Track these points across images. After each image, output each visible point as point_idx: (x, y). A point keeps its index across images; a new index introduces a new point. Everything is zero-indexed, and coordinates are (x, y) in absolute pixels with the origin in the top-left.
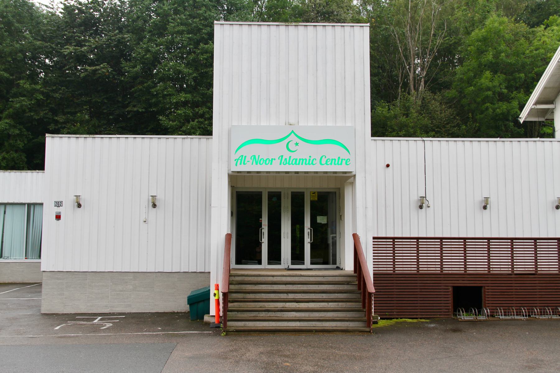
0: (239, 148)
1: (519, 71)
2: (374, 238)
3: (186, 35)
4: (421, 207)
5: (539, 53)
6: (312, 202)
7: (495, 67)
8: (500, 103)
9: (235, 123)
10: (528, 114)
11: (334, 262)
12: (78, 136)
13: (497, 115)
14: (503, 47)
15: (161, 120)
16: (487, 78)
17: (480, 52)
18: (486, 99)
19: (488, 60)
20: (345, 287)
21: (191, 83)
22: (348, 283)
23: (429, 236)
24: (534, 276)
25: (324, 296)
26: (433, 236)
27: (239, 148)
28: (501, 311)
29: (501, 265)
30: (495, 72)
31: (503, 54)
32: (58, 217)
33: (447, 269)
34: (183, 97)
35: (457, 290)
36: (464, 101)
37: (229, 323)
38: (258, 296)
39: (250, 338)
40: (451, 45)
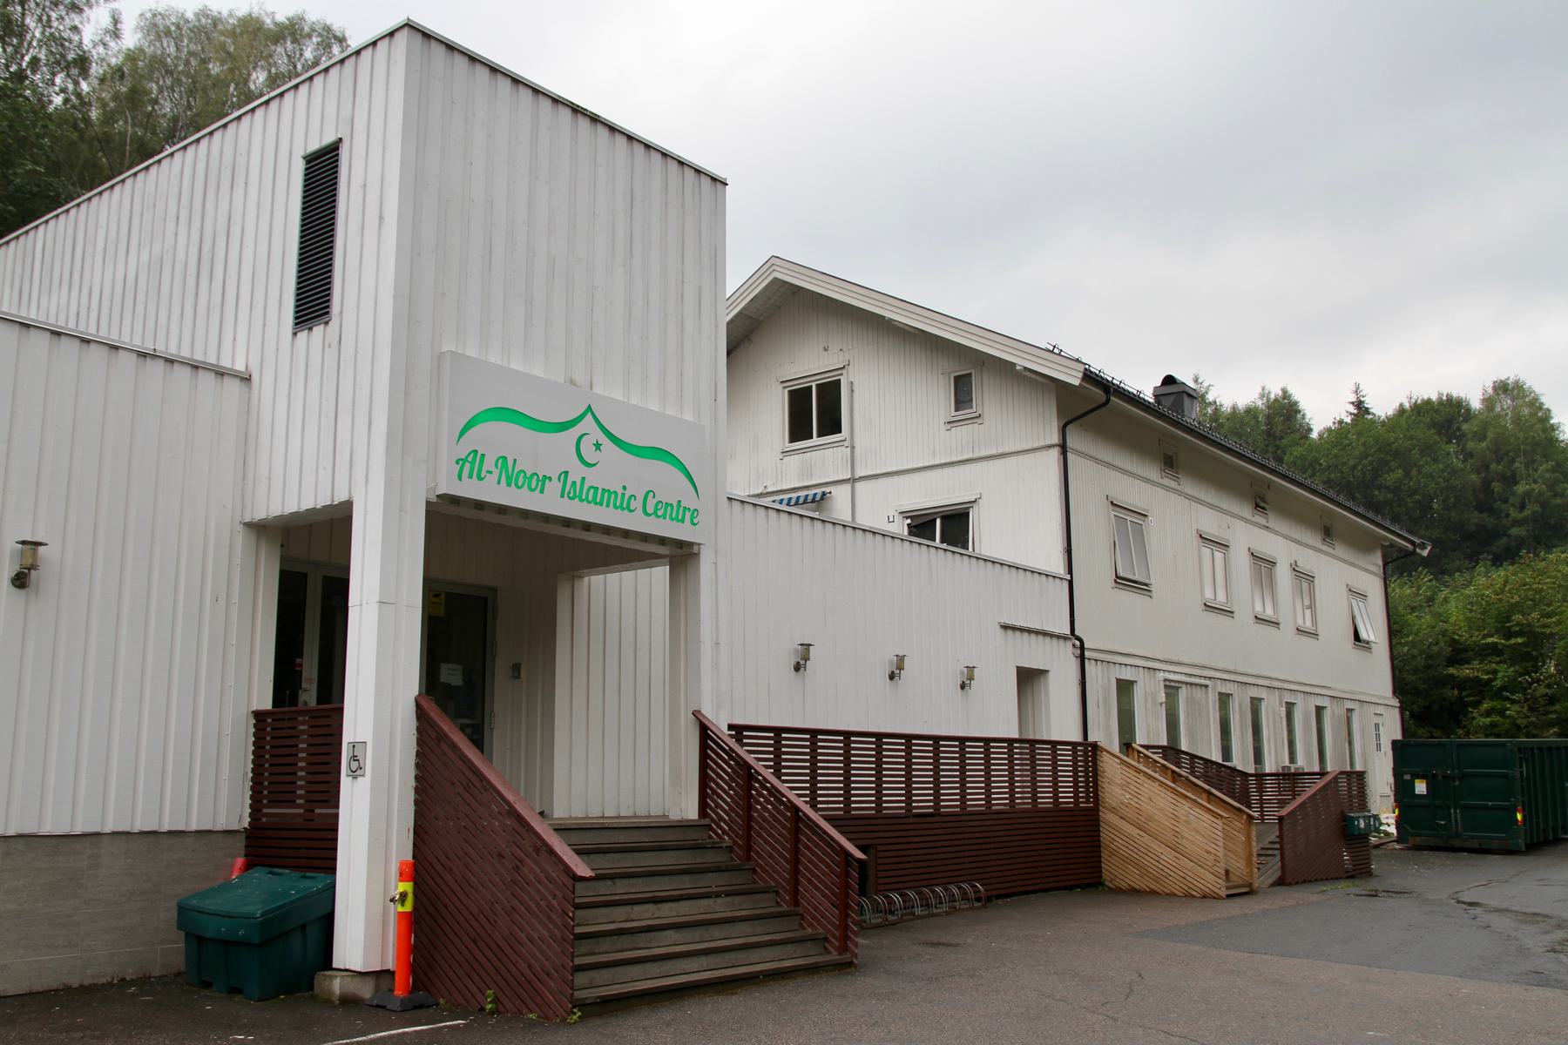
9: (447, 347)
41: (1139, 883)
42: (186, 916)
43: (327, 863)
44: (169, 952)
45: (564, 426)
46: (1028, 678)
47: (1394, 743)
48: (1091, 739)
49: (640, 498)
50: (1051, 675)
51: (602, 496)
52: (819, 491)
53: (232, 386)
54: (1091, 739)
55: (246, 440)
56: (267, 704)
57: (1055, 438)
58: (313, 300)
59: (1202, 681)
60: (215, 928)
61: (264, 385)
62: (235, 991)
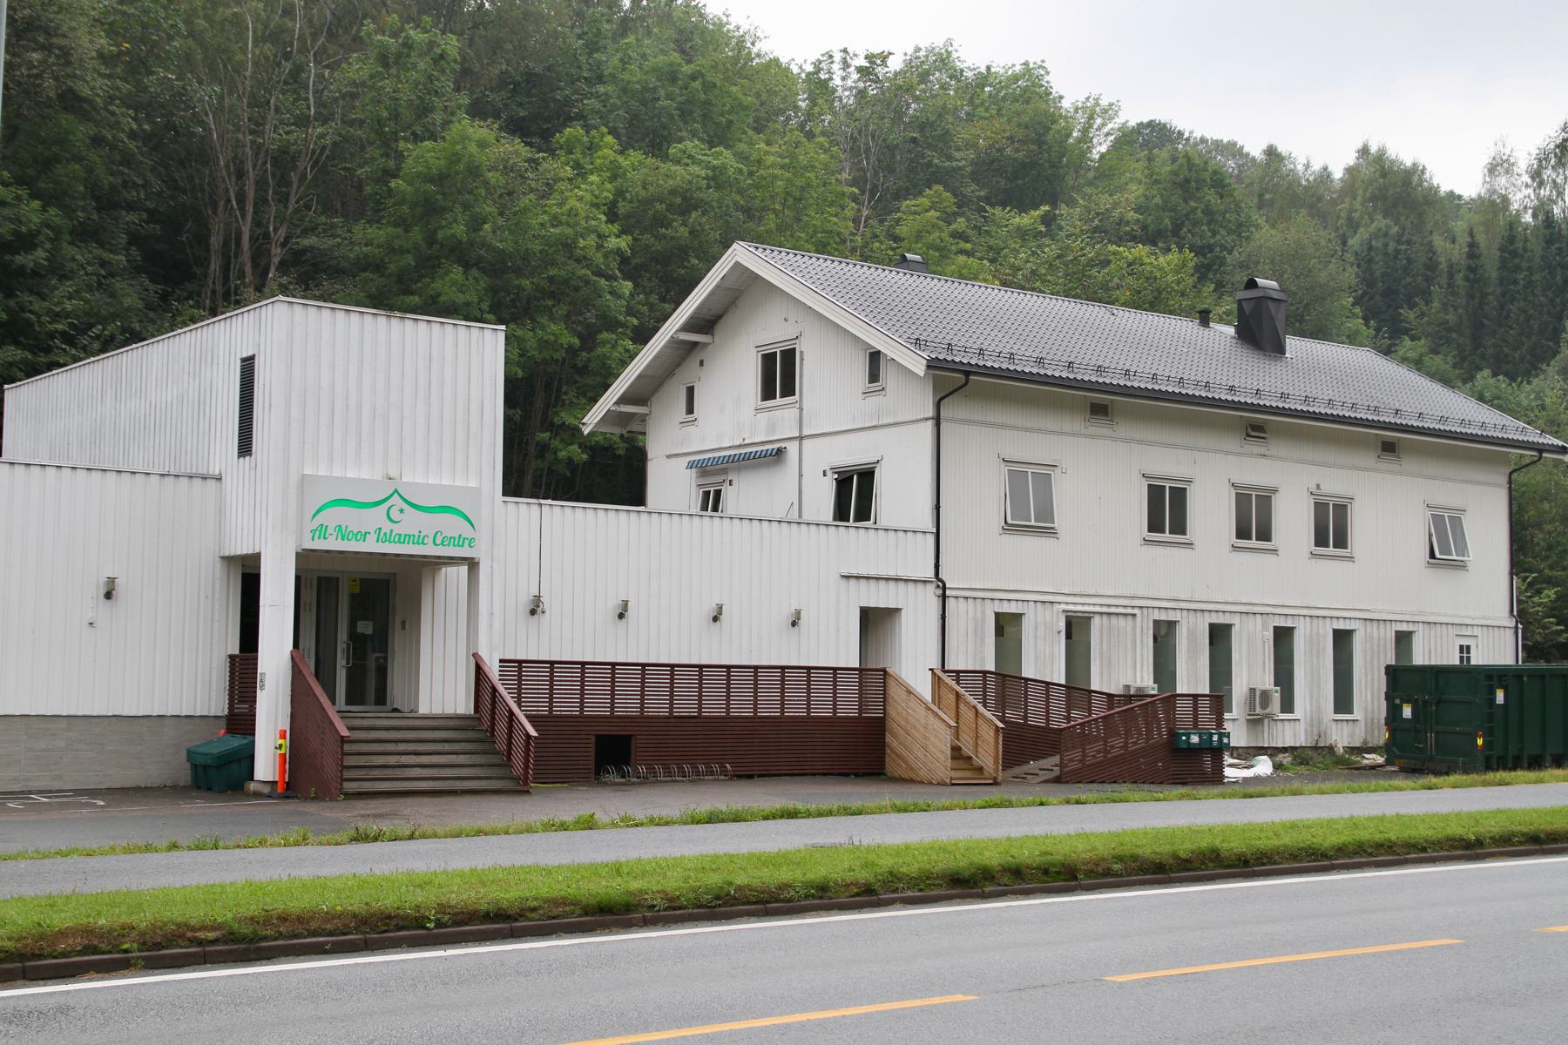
0: (318, 511)
1: (519, 272)
4: (533, 612)
6: (353, 596)
9: (308, 471)
11: (381, 699)
14: (488, 208)
16: (454, 283)
19: (453, 236)
20: (471, 735)
24: (697, 721)
25: (447, 747)
27: (318, 511)
28: (659, 768)
29: (657, 707)
35: (600, 739)
42: (191, 754)
43: (251, 731)
44: (184, 775)
46: (874, 622)
47: (1388, 668)
51: (408, 538)
52: (776, 446)
53: (211, 484)
55: (221, 511)
56: (236, 651)
57: (930, 412)
58: (245, 447)
59: (1129, 611)
60: (200, 760)
61: (227, 480)
62: (210, 789)
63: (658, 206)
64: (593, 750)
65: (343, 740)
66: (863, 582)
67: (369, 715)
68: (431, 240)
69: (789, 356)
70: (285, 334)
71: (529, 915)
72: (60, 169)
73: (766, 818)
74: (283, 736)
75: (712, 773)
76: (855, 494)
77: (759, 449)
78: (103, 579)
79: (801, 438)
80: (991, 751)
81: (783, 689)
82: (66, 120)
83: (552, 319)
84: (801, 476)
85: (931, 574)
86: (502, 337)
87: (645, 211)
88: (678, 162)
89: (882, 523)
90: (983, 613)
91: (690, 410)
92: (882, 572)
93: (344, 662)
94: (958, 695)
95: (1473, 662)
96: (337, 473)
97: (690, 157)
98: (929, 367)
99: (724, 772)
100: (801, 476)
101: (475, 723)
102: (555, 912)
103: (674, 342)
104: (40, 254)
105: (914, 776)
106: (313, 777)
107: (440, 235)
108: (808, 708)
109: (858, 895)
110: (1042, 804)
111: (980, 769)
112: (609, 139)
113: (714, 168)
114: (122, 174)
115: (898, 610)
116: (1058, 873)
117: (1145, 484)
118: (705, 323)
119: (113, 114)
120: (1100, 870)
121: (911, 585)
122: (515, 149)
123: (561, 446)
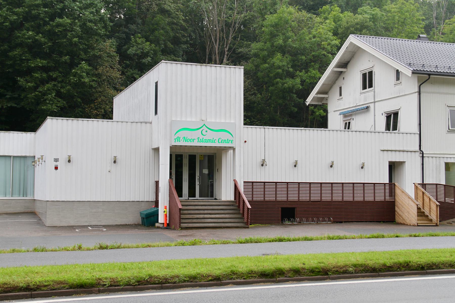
0: (177, 132)
1: (303, 54)
2: (244, 182)
3: (42, 9)
5: (315, 41)
7: (283, 50)
8: (287, 80)
9: (173, 119)
10: (312, 100)
11: (212, 196)
12: (68, 118)
13: (284, 89)
14: (290, 34)
15: (19, 81)
16: (278, 59)
17: (273, 36)
18: (278, 75)
19: (279, 44)
20: (232, 207)
21: (46, 51)
22: (233, 205)
23: (257, 181)
25: (222, 212)
26: (272, 181)
27: (177, 132)
28: (304, 219)
29: (304, 197)
30: (284, 53)
31: (290, 40)
32: (56, 168)
33: (279, 199)
34: (40, 62)
36: (260, 74)
37: (182, 224)
38: (189, 212)
39: (197, 230)
40: (246, 20)
41: (402, 222)
44: (138, 220)
45: (198, 129)
46: (393, 167)
48: (424, 183)
49: (217, 140)
50: (406, 163)
52: (366, 106)
53: (148, 125)
54: (424, 183)
57: (417, 90)
58: (156, 113)
63: (351, 29)
64: (280, 214)
65: (180, 209)
66: (389, 152)
67: (206, 201)
68: (272, 46)
69: (371, 73)
70: (168, 74)
71: (43, 288)
72: (156, 32)
73: (270, 241)
74: (166, 208)
75: (325, 221)
76: (392, 121)
77: (361, 107)
78: (113, 157)
79: (375, 102)
80: (435, 214)
81: (353, 191)
82: (159, 17)
83: (314, 69)
84: (375, 115)
85: (418, 149)
86: (242, 71)
87: (347, 31)
88: (361, 14)
89: (402, 130)
90: (440, 162)
91: (341, 95)
92: (397, 149)
93: (198, 183)
94: (423, 193)
95: (388, 182)
96: (184, 119)
97: (366, 12)
98: (413, 73)
99: (329, 220)
100: (375, 115)
101: (235, 203)
102: (56, 287)
103: (333, 72)
104: (149, 59)
105: (405, 223)
106: (179, 221)
107: (275, 44)
108: (354, 198)
109: (211, 280)
110: (397, 237)
111: (431, 220)
112: (338, 8)
113: (373, 15)
114: (181, 33)
115: (404, 162)
116: (319, 272)
117: (448, 109)
118: (344, 64)
119: (177, 15)
120: (342, 270)
121: (409, 153)
122: (304, 14)
123: (317, 111)
